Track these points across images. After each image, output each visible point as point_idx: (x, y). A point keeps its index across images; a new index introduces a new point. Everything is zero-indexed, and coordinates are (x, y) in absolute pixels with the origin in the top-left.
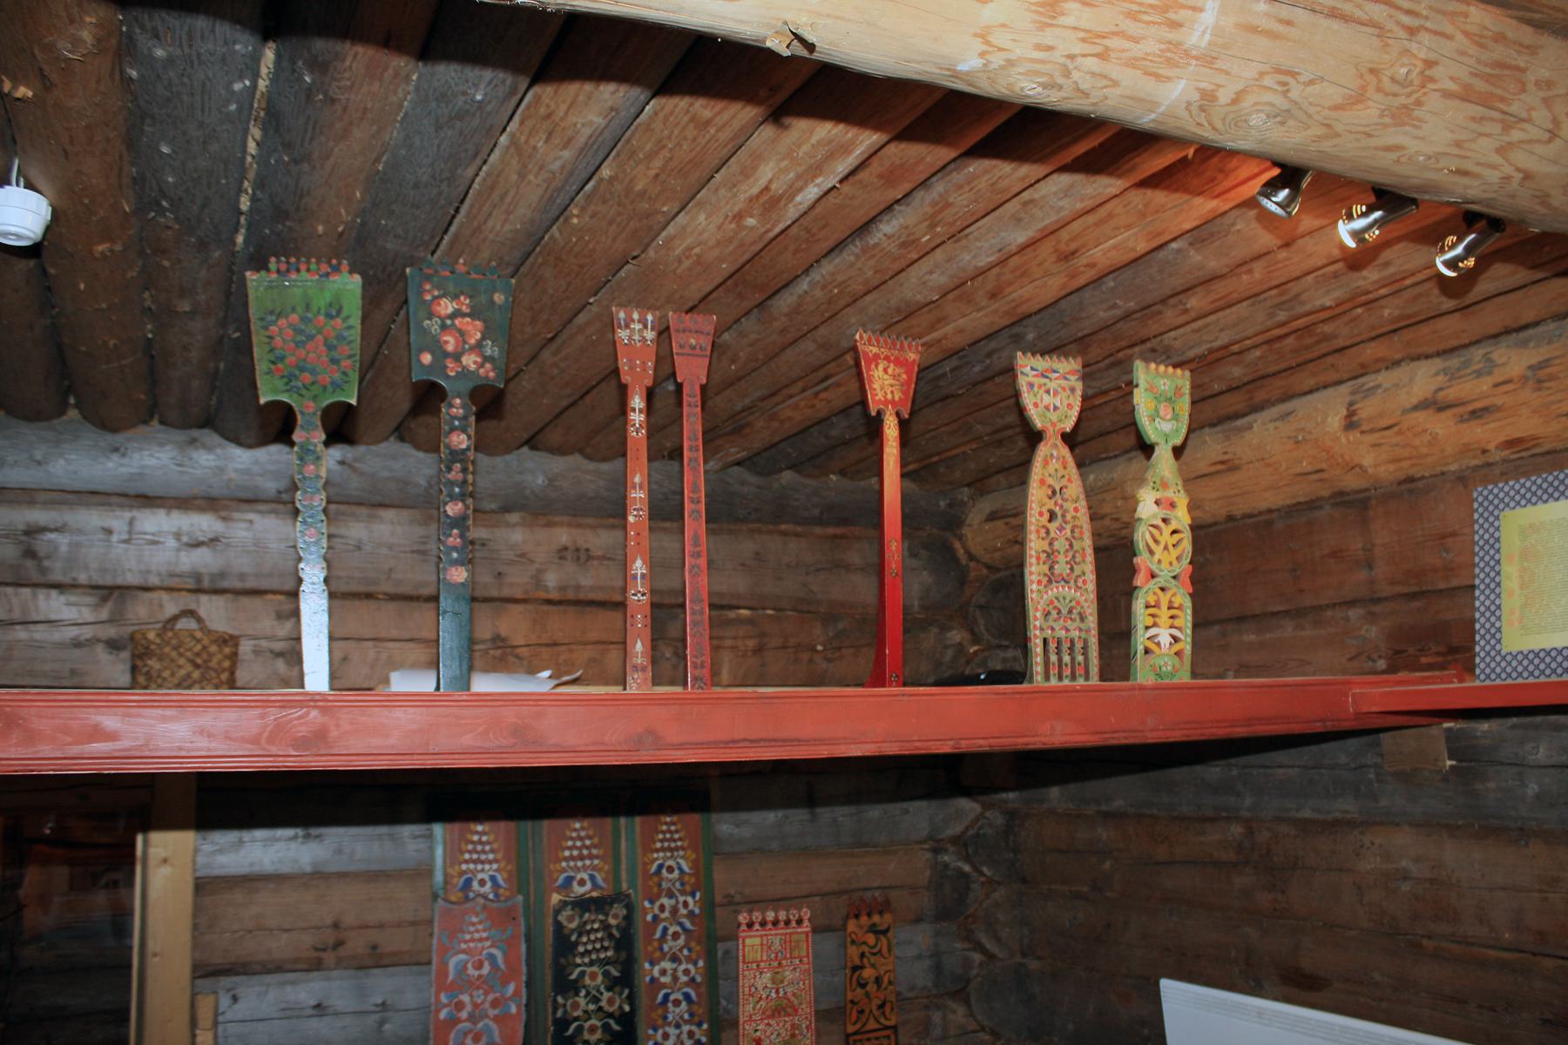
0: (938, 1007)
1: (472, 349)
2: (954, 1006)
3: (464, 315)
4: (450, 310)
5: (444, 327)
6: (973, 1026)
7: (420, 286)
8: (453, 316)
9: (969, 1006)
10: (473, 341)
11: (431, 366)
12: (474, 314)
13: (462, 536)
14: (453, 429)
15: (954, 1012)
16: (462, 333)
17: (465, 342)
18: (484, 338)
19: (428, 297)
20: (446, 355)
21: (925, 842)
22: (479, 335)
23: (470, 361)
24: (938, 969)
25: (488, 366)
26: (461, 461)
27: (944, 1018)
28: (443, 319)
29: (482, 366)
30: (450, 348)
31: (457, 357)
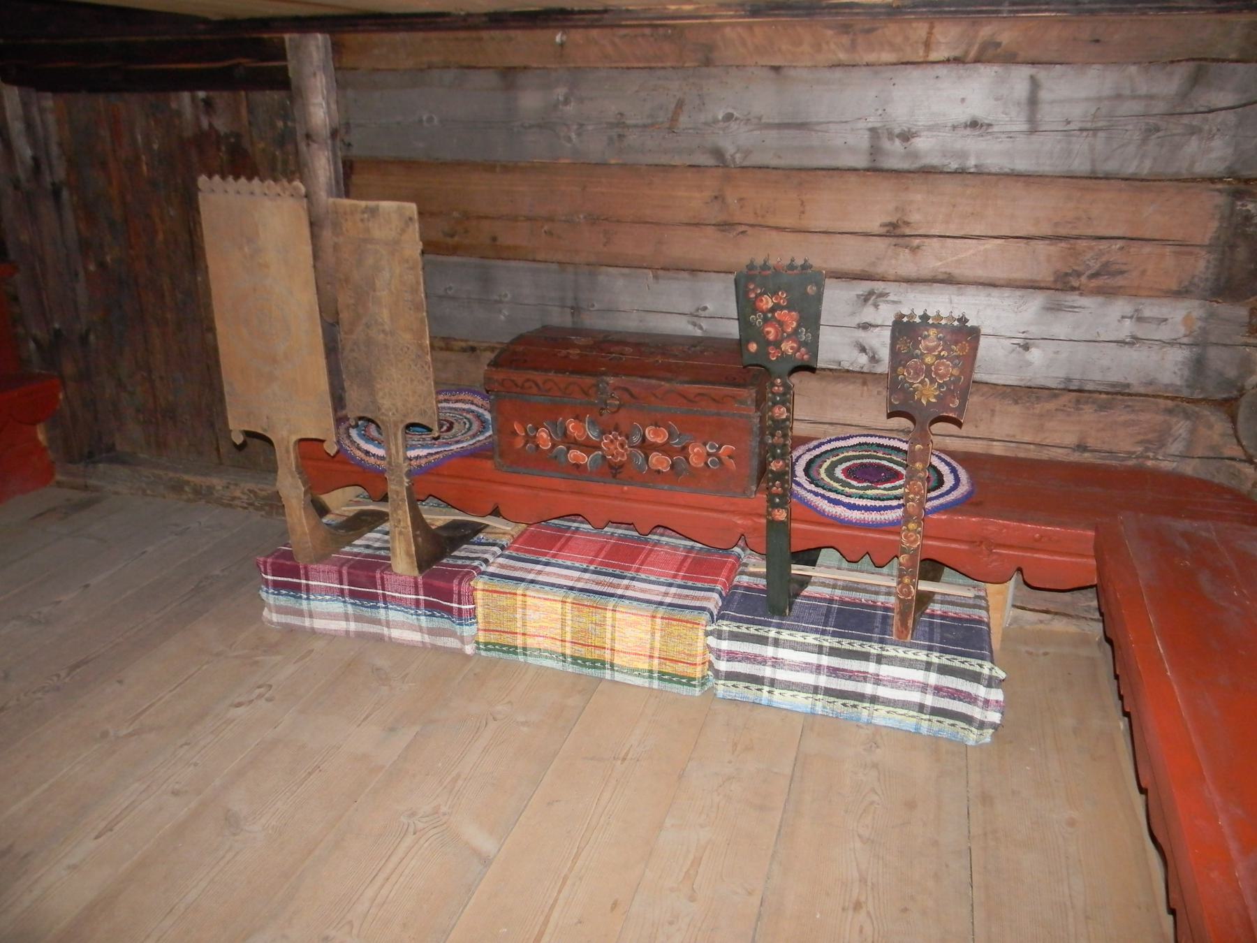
0: (1187, 416)
1: (789, 336)
2: (1213, 419)
3: (782, 308)
4: (770, 305)
5: (766, 320)
6: (1236, 451)
7: (746, 286)
8: (773, 310)
9: (1233, 419)
10: (790, 330)
11: (756, 353)
12: (790, 307)
13: (782, 487)
14: (775, 404)
15: (1210, 427)
16: (781, 323)
17: (783, 331)
18: (799, 326)
19: (752, 296)
20: (769, 343)
21: (1221, 179)
22: (795, 324)
23: (787, 347)
24: (1198, 366)
25: (803, 350)
26: (781, 429)
27: (1193, 431)
28: (765, 313)
29: (798, 350)
30: (771, 337)
31: (777, 344)
